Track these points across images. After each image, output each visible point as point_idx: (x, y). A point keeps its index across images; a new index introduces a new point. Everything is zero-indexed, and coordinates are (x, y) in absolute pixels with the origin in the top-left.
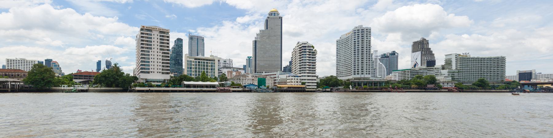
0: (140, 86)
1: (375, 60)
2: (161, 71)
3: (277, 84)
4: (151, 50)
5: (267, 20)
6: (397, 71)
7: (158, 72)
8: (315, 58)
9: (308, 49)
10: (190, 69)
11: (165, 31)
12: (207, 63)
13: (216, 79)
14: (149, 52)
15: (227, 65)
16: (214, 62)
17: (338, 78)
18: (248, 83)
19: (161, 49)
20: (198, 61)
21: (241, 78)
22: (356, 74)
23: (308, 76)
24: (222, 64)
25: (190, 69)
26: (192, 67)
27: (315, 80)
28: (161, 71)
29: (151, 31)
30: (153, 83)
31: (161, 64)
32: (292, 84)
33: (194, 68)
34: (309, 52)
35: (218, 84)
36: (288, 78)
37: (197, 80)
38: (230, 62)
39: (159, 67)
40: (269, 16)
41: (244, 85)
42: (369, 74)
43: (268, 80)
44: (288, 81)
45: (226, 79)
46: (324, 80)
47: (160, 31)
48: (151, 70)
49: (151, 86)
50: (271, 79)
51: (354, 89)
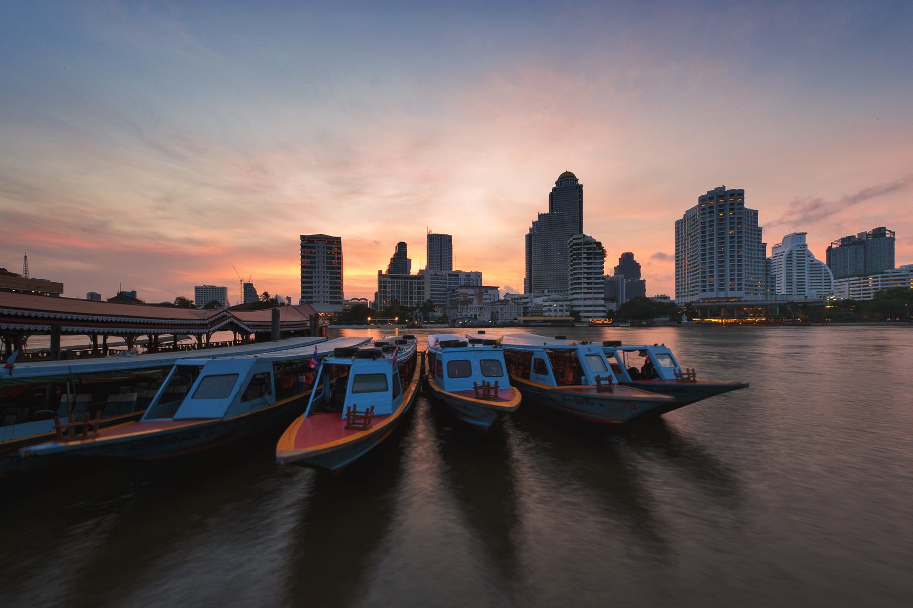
2: (328, 300)
6: (847, 279)
7: (324, 302)
9: (584, 248)
12: (411, 283)
14: (311, 273)
15: (471, 281)
19: (328, 268)
21: (459, 306)
22: (707, 291)
23: (585, 299)
24: (462, 280)
28: (328, 300)
32: (552, 314)
33: (415, 292)
34: (588, 254)
42: (740, 289)
43: (512, 307)
44: (545, 309)
48: (314, 300)
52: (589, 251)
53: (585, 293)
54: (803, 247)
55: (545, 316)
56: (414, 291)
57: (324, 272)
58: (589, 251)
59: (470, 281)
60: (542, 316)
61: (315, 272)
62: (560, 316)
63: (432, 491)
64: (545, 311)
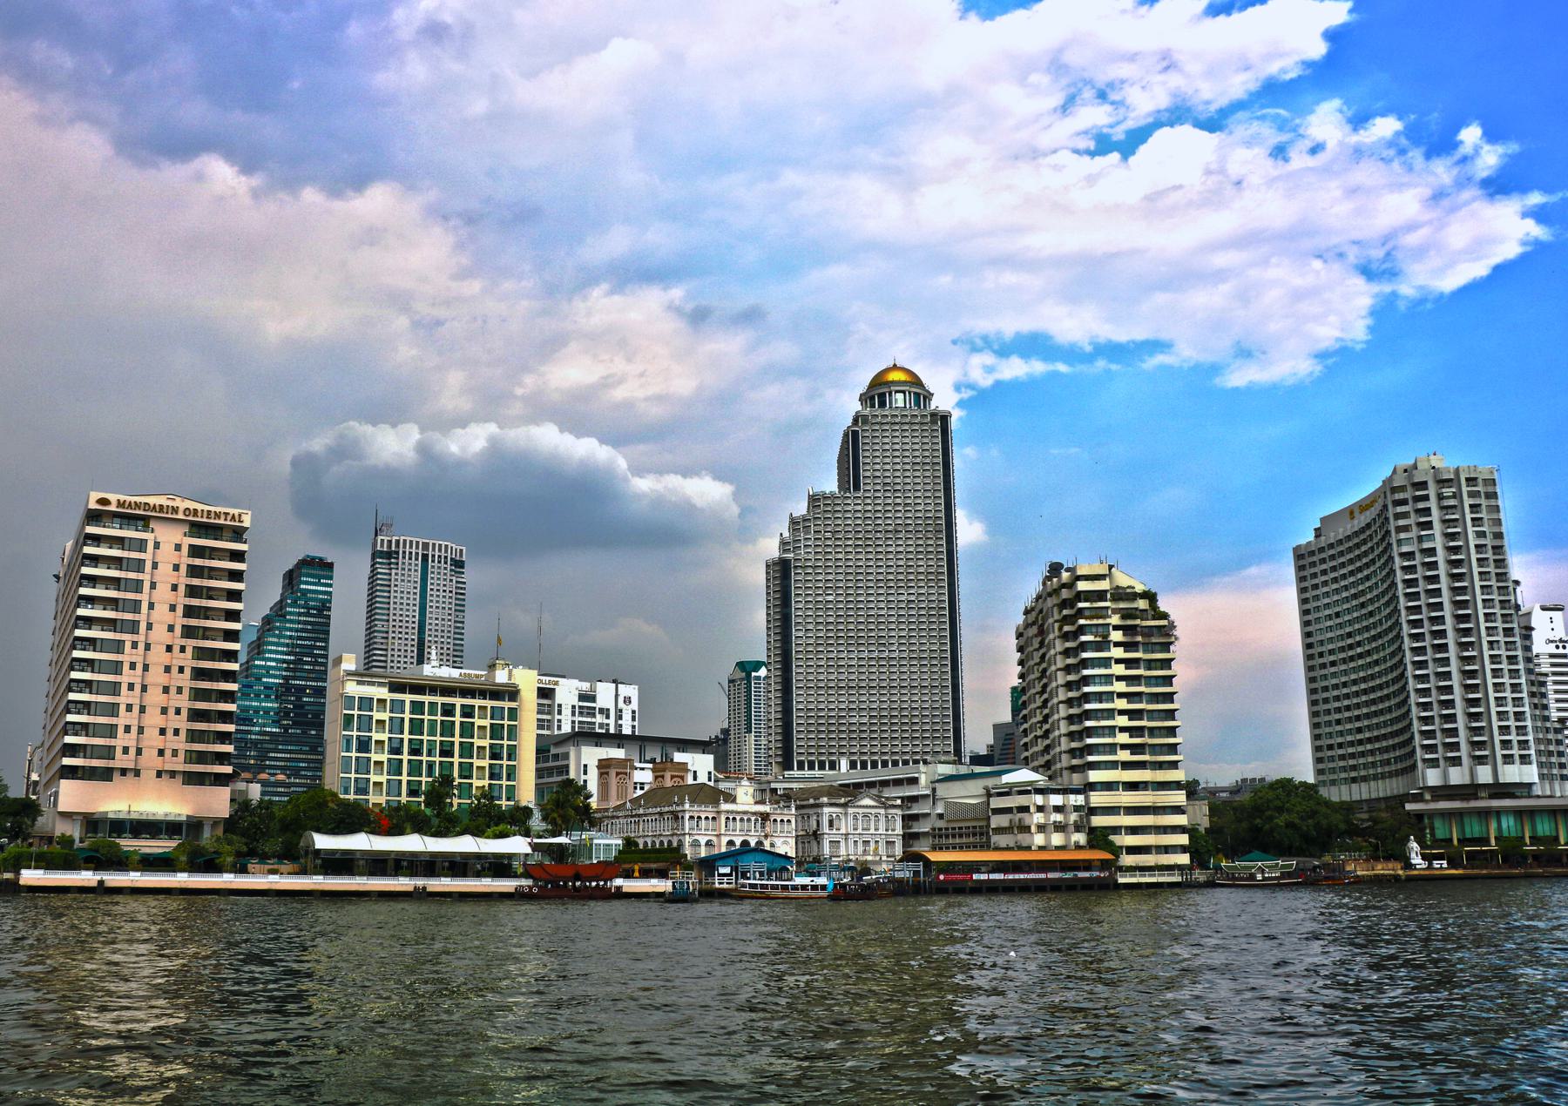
0: (48, 863)
1: (1553, 665)
3: (922, 847)
4: (135, 637)
5: (855, 434)
7: (159, 774)
8: (1167, 663)
10: (359, 751)
11: (222, 521)
13: (517, 820)
14: (118, 647)
15: (599, 719)
16: (513, 705)
17: (1323, 792)
18: (731, 843)
19: (189, 632)
20: (408, 698)
21: (687, 806)
23: (1133, 786)
24: (567, 711)
25: (359, 751)
26: (370, 738)
27: (1178, 810)
28: (179, 765)
29: (140, 523)
30: (127, 844)
31: (182, 723)
35: (529, 850)
36: (996, 803)
37: (394, 821)
38: (621, 700)
39: (172, 742)
40: (867, 411)
41: (703, 853)
43: (865, 816)
44: (997, 821)
45: (587, 818)
46: (1238, 809)
47: (193, 525)
48: (120, 761)
49: (120, 862)
50: (882, 811)
51: (1436, 864)
52: (1130, 622)
53: (1127, 765)
54: (1561, 645)
55: (997, 849)
56: (477, 742)
57: (169, 649)
58: (1130, 622)
59: (594, 715)
60: (986, 846)
61: (135, 645)
62: (1057, 848)
63: (1427, 1086)
64: (1000, 830)
